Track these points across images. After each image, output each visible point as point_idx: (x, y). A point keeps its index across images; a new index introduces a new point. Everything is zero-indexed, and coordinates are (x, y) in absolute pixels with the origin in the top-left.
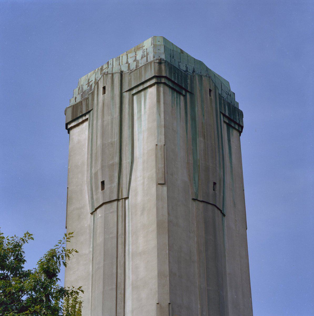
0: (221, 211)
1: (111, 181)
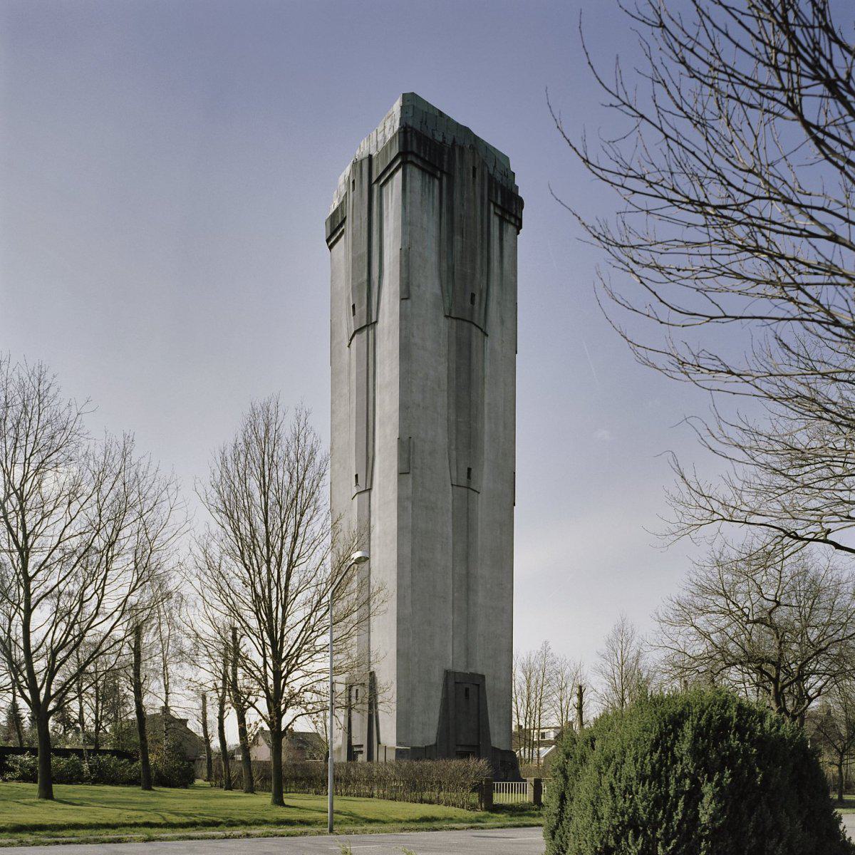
0: (482, 330)
1: (361, 304)
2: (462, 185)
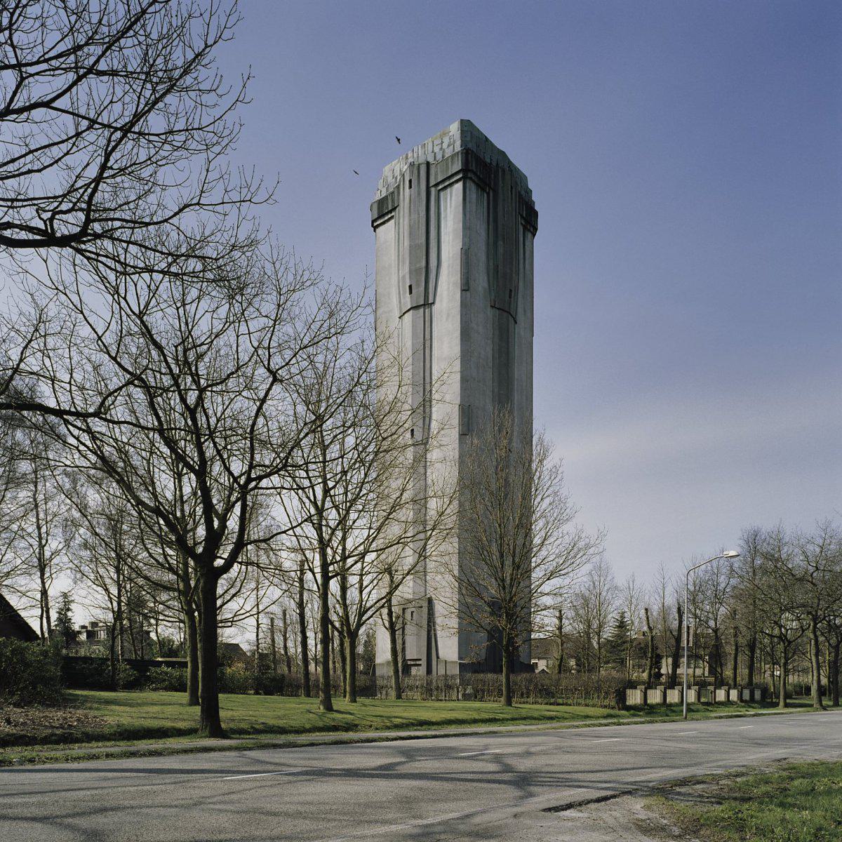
1: (418, 286)
2: (504, 200)
